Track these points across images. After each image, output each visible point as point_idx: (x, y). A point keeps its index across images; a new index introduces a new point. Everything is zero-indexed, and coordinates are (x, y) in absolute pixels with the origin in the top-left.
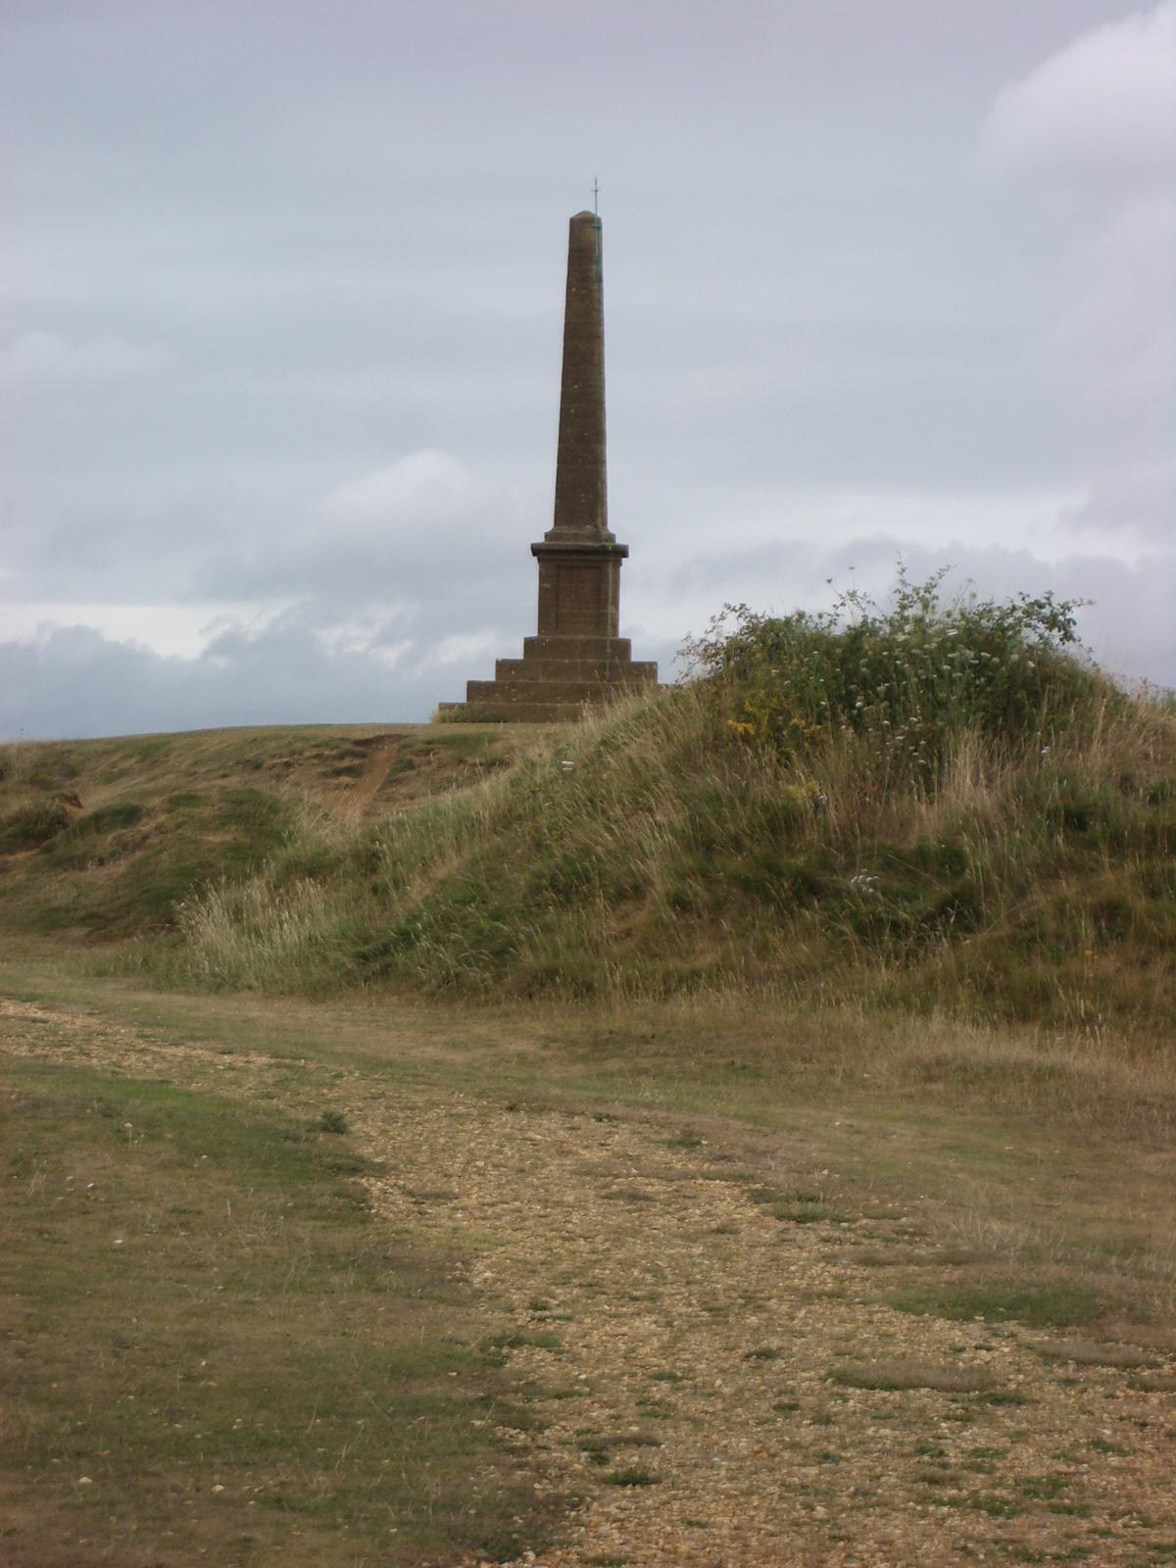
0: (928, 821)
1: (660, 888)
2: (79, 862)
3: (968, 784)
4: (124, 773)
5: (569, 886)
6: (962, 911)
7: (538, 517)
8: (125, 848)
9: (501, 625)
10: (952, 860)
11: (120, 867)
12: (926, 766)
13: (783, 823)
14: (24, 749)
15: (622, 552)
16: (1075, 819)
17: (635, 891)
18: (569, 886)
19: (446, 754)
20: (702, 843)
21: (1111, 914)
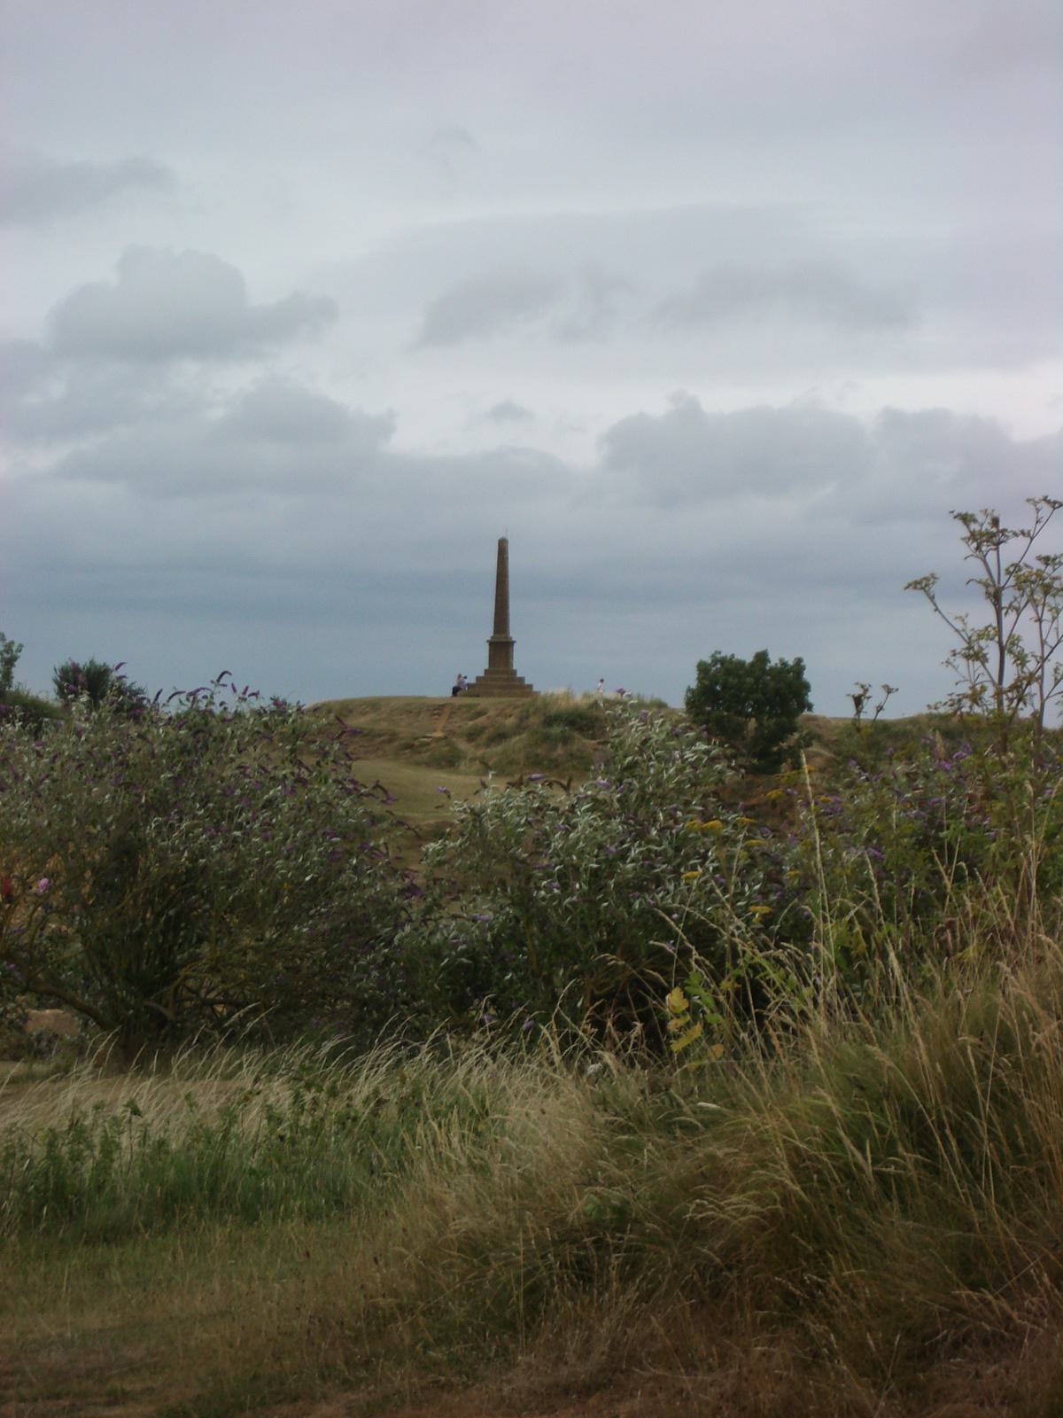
0: (554, 755)
1: (522, 763)
2: (419, 753)
3: (560, 750)
4: (367, 713)
5: (511, 763)
6: (557, 766)
7: (488, 632)
8: (428, 750)
9: (476, 663)
10: (557, 760)
11: (428, 754)
12: (554, 748)
13: (537, 755)
14: (336, 702)
15: (513, 642)
16: (571, 755)
17: (518, 764)
18: (511, 763)
19: (465, 709)
20: (527, 758)
21: (574, 766)
